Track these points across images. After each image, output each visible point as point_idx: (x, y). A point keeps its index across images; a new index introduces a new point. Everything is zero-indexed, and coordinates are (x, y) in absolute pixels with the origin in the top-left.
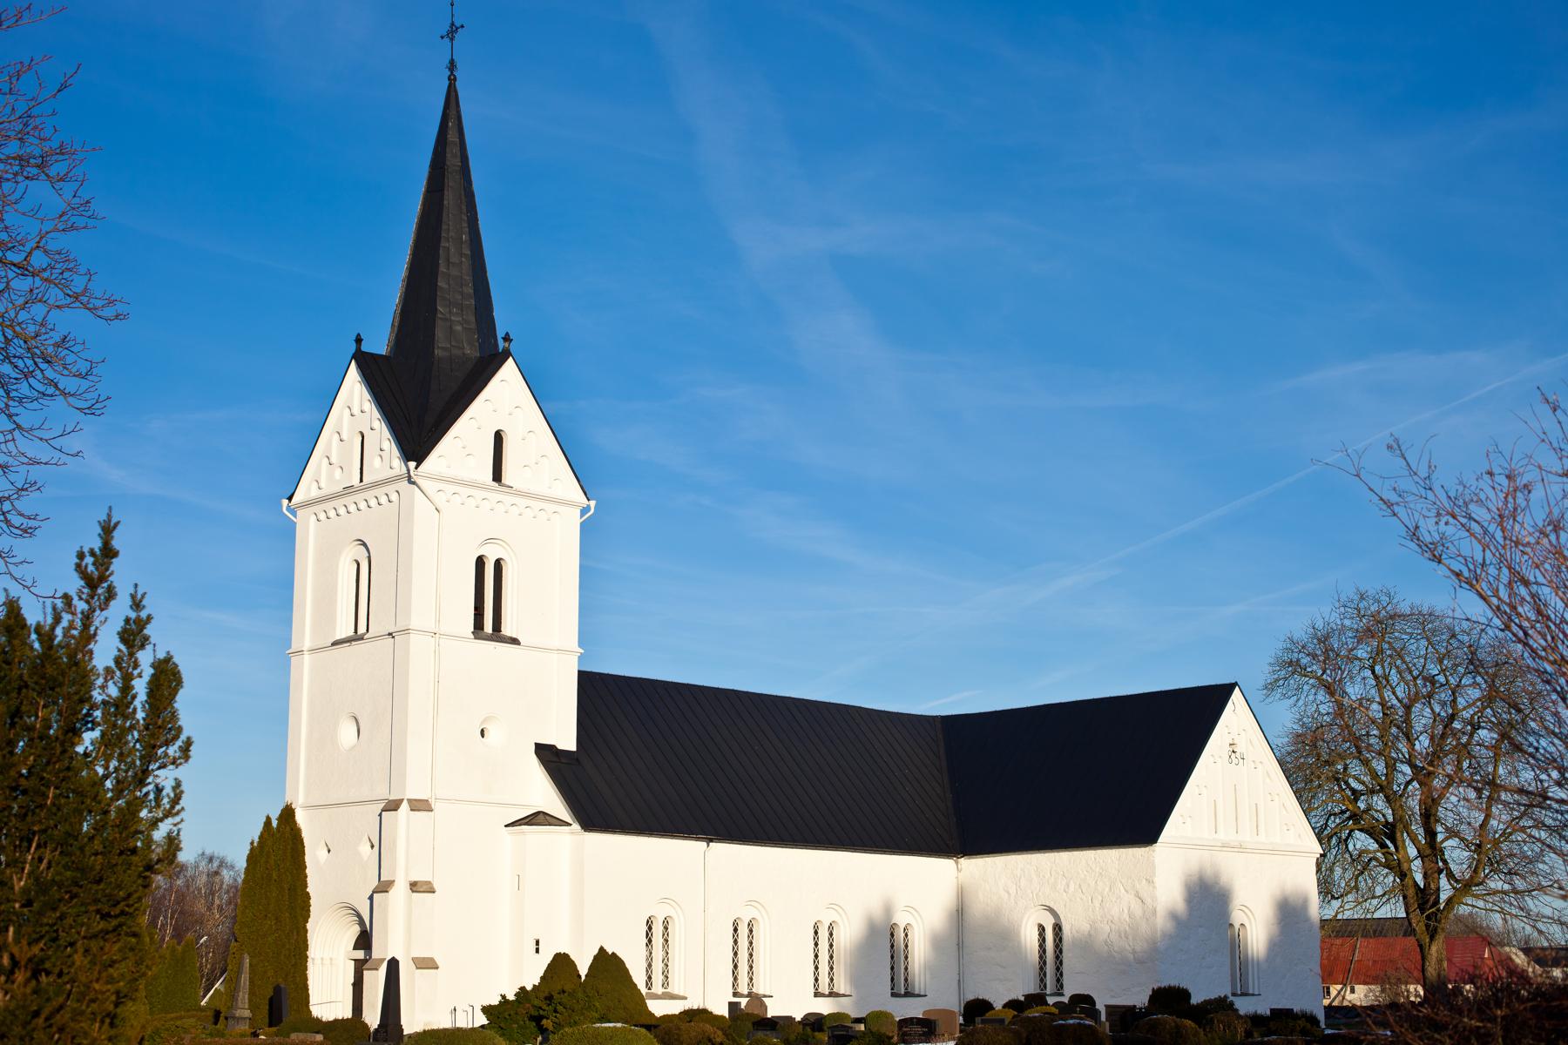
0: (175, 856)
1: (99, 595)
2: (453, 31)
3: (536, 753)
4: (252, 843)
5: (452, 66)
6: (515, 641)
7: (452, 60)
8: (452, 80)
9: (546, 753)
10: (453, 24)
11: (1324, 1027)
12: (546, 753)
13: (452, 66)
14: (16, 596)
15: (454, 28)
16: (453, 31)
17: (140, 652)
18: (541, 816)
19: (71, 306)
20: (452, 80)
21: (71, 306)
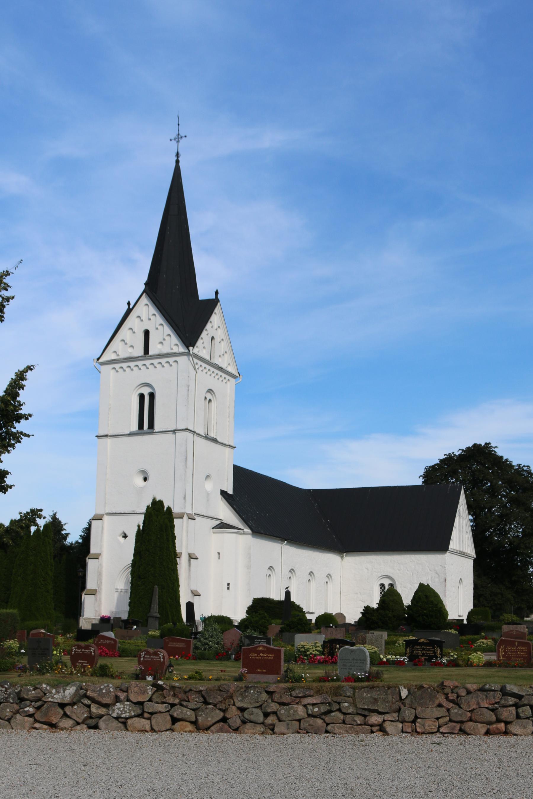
0: (124, 621)
1: (156, 654)
2: (178, 138)
3: (221, 494)
4: (139, 526)
5: (178, 155)
6: (217, 293)
7: (178, 152)
8: (177, 162)
9: (224, 493)
10: (178, 135)
11: (388, 657)
12: (224, 493)
13: (178, 155)
14: (27, 377)
15: (179, 137)
16: (178, 138)
17: (5, 309)
18: (94, 523)
19: (131, 307)
20: (177, 162)
21: (131, 307)
